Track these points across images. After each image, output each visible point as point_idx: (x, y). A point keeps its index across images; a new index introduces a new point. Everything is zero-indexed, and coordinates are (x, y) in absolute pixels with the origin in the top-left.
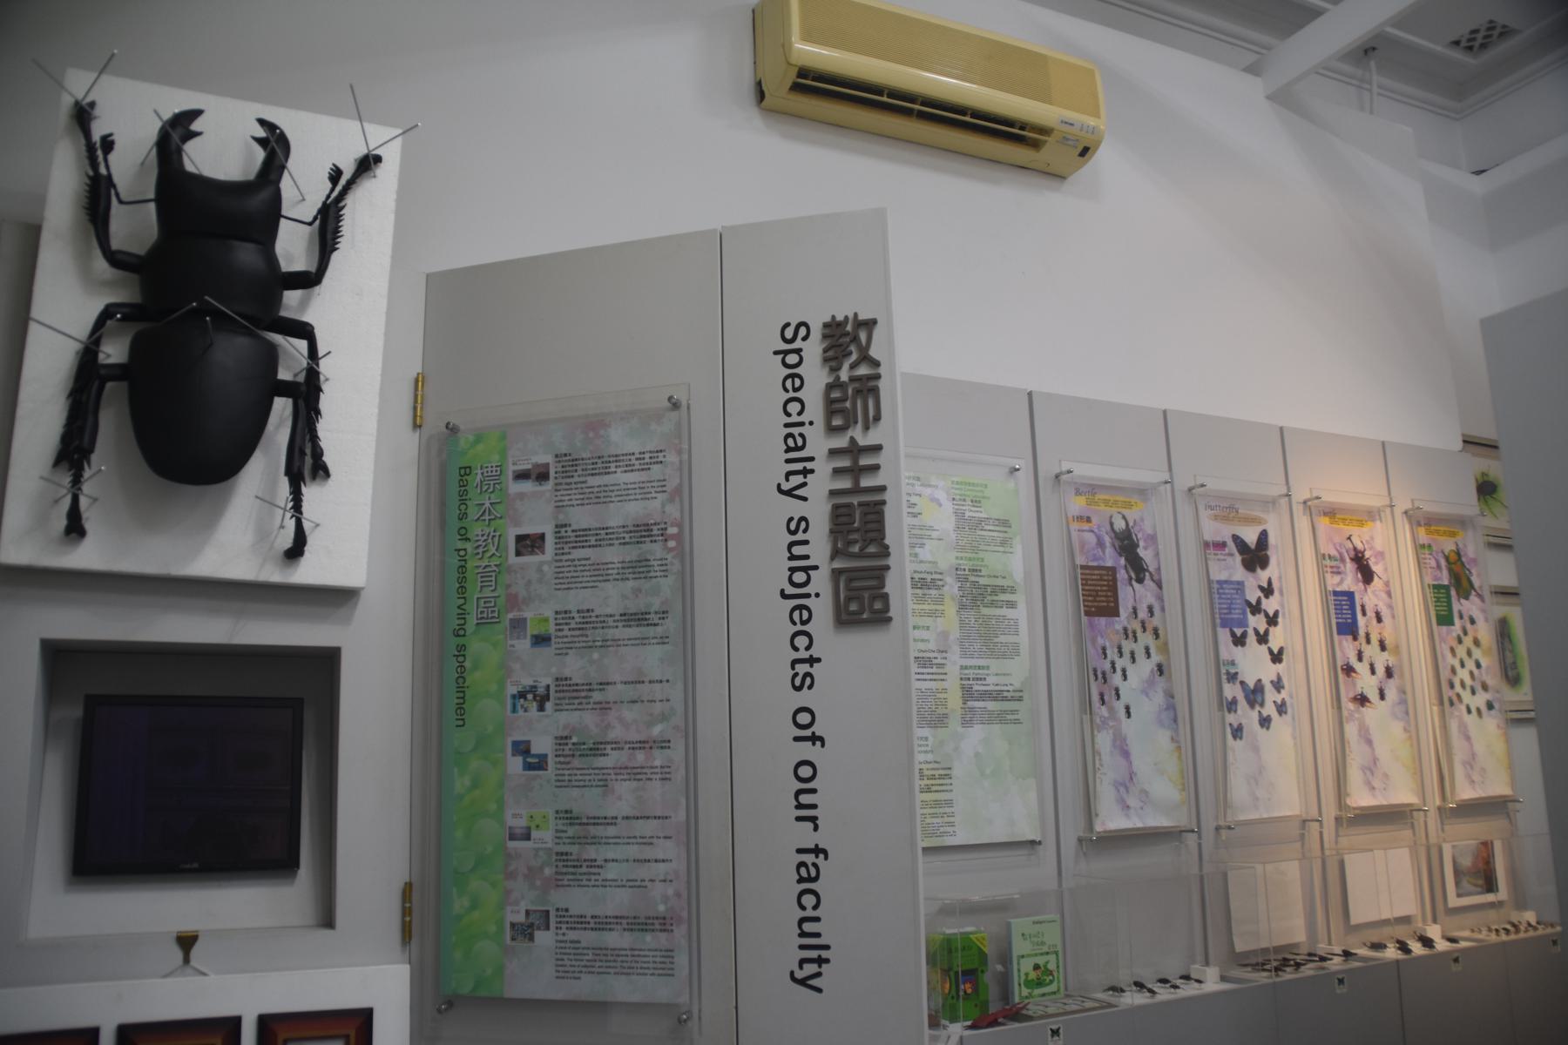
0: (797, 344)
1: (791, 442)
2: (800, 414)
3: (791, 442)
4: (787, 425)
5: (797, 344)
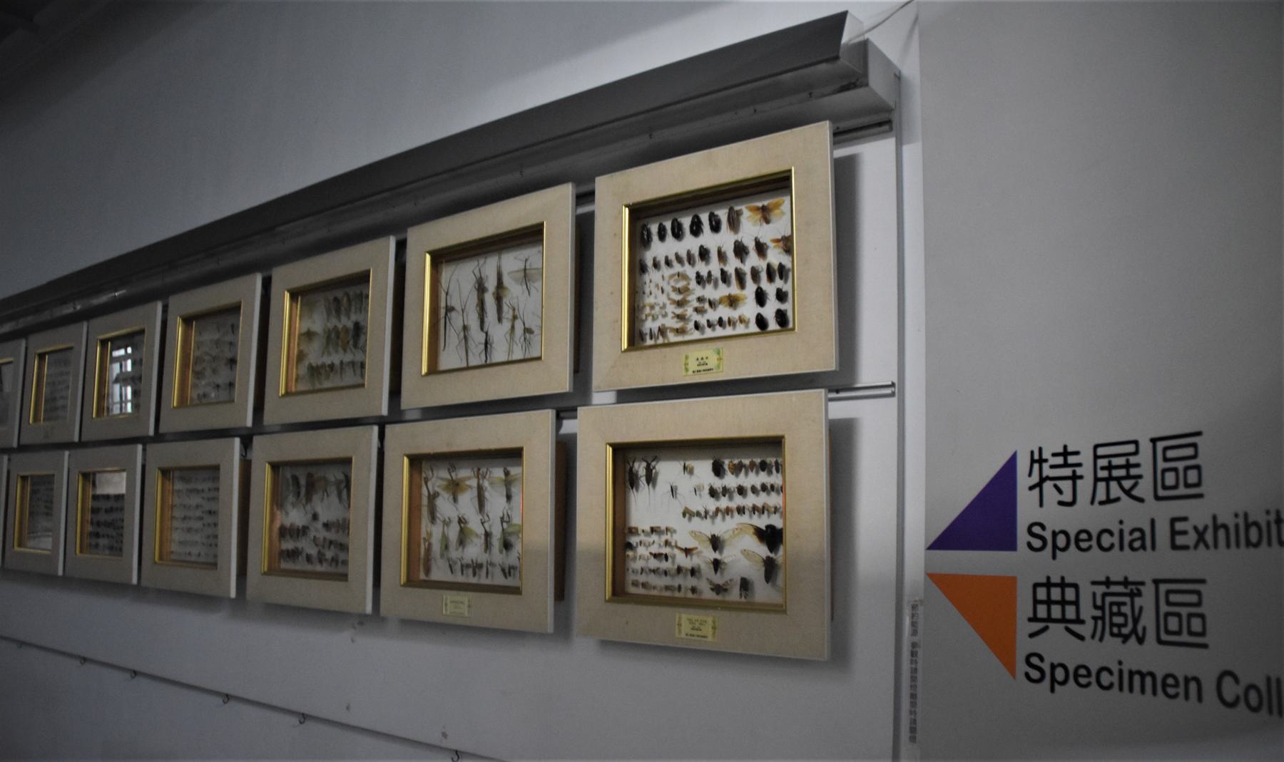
0: (1048, 535)
1: (1137, 544)
2: (1111, 673)
3: (1137, 544)
4: (1122, 548)
5: (1046, 667)
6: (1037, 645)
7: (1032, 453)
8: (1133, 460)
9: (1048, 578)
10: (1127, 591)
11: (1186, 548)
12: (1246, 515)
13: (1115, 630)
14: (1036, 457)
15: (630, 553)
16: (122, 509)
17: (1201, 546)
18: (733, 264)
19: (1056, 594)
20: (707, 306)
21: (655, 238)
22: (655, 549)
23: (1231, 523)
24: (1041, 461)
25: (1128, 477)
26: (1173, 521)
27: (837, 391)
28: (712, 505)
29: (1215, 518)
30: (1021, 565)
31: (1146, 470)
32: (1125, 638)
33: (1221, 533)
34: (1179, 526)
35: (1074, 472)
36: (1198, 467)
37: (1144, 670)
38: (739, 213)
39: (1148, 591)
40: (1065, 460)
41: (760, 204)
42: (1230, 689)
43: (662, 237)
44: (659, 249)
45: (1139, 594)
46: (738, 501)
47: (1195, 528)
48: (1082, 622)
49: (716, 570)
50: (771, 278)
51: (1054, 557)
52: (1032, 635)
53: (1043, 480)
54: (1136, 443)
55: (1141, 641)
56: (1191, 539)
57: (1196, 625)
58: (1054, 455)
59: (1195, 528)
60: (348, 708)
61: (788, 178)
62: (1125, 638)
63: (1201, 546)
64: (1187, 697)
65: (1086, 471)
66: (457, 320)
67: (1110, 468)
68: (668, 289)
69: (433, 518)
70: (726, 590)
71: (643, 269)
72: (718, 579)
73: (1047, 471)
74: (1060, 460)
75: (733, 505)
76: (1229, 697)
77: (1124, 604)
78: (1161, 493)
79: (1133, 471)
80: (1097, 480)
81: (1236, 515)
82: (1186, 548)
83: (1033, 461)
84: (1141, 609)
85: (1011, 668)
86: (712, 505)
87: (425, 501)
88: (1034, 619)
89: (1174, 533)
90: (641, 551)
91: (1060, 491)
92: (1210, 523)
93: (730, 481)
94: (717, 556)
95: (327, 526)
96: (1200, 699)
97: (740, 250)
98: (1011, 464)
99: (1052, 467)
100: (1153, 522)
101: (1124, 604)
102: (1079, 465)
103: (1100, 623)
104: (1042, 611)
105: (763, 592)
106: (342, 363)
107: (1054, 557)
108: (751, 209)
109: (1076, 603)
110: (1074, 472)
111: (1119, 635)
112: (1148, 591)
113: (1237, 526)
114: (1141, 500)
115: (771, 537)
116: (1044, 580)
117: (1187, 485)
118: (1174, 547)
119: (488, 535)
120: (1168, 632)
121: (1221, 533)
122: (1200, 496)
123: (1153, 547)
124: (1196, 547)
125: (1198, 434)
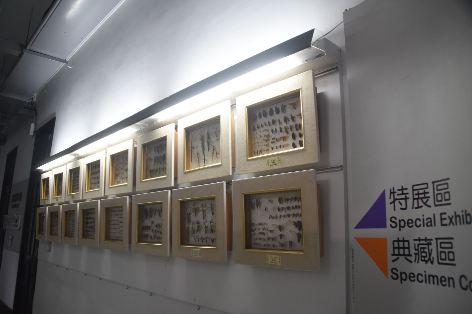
0: (397, 221)
2: (422, 276)
3: (429, 224)
4: (424, 226)
6: (395, 265)
7: (391, 189)
8: (426, 190)
9: (398, 238)
10: (426, 243)
11: (446, 225)
12: (466, 211)
13: (423, 259)
14: (392, 191)
15: (252, 233)
16: (94, 222)
17: (451, 224)
18: (284, 125)
19: (401, 244)
20: (276, 141)
21: (258, 118)
22: (261, 231)
23: (461, 214)
24: (394, 193)
25: (425, 197)
26: (441, 214)
27: (322, 170)
28: (279, 214)
29: (455, 213)
30: (388, 233)
31: (431, 195)
32: (427, 262)
33: (458, 218)
34: (443, 216)
35: (406, 196)
36: (448, 192)
37: (434, 275)
38: (285, 106)
39: (434, 242)
40: (403, 192)
41: (292, 102)
42: (465, 283)
43: (260, 117)
44: (260, 121)
45: (431, 244)
46: (288, 212)
47: (449, 217)
48: (411, 255)
49: (281, 238)
50: (297, 130)
51: (400, 230)
52: (393, 261)
53: (395, 200)
54: (427, 184)
55: (432, 263)
56: (447, 222)
57: (451, 256)
58: (399, 190)
59: (449, 217)
60: (164, 290)
61: (299, 93)
62: (427, 262)
63: (451, 224)
64: (449, 286)
65: (410, 196)
66: (195, 151)
67: (418, 194)
68: (263, 136)
69: (189, 221)
70: (285, 246)
71: (254, 129)
72: (282, 241)
73: (396, 197)
74: (400, 192)
75: (286, 214)
76: (464, 286)
77: (425, 248)
78: (437, 203)
79: (427, 195)
80: (414, 199)
81: (462, 211)
82: (446, 225)
83: (391, 193)
84: (432, 250)
85: (386, 274)
86: (279, 214)
87: (186, 216)
88: (394, 255)
89: (442, 219)
90: (257, 232)
91: (401, 204)
92: (453, 214)
93: (285, 205)
94: (281, 233)
95: (156, 226)
96: (454, 286)
97: (286, 120)
98: (383, 194)
99: (398, 195)
100: (434, 215)
101: (425, 248)
102: (408, 194)
103: (417, 256)
104: (396, 251)
105: (298, 245)
106: (160, 168)
107: (400, 230)
108: (289, 104)
109: (408, 248)
110: (406, 196)
111: (424, 261)
112: (434, 242)
113: (463, 215)
114: (430, 206)
115: (299, 225)
116: (397, 239)
117: (446, 200)
118: (442, 225)
119: (206, 227)
120: (442, 259)
121: (458, 218)
122: (450, 204)
123: (435, 225)
124: (449, 225)
125: (448, 179)
